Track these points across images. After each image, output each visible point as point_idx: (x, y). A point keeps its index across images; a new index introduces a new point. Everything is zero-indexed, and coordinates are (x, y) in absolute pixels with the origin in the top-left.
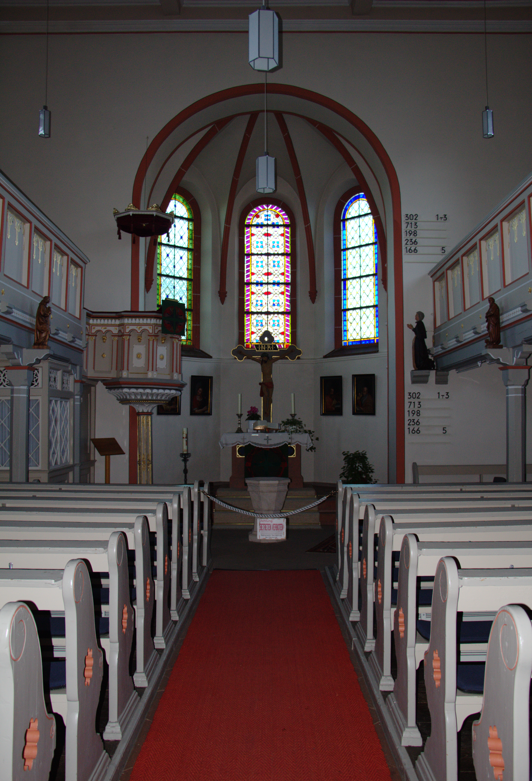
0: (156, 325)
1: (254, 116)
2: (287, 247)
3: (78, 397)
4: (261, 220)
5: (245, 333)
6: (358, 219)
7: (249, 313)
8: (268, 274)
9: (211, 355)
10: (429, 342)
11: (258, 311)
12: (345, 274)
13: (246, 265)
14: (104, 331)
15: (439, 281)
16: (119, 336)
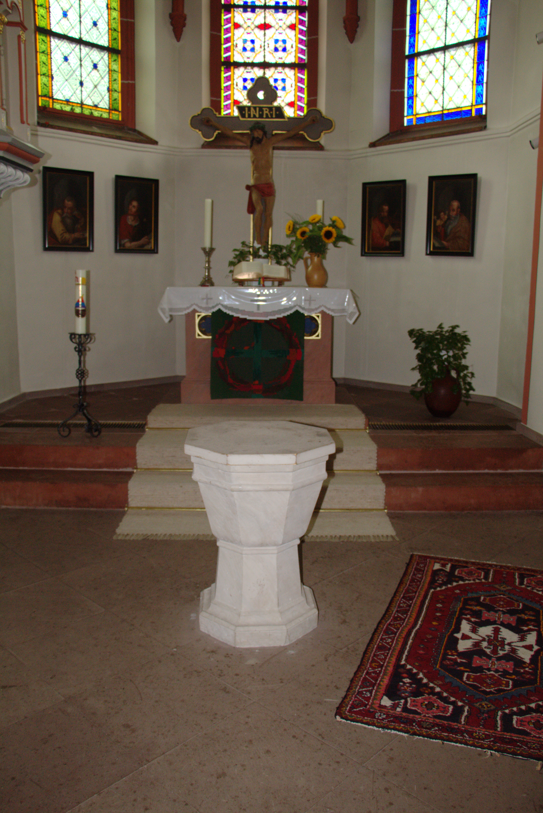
7: (230, 65)
11: (247, 61)
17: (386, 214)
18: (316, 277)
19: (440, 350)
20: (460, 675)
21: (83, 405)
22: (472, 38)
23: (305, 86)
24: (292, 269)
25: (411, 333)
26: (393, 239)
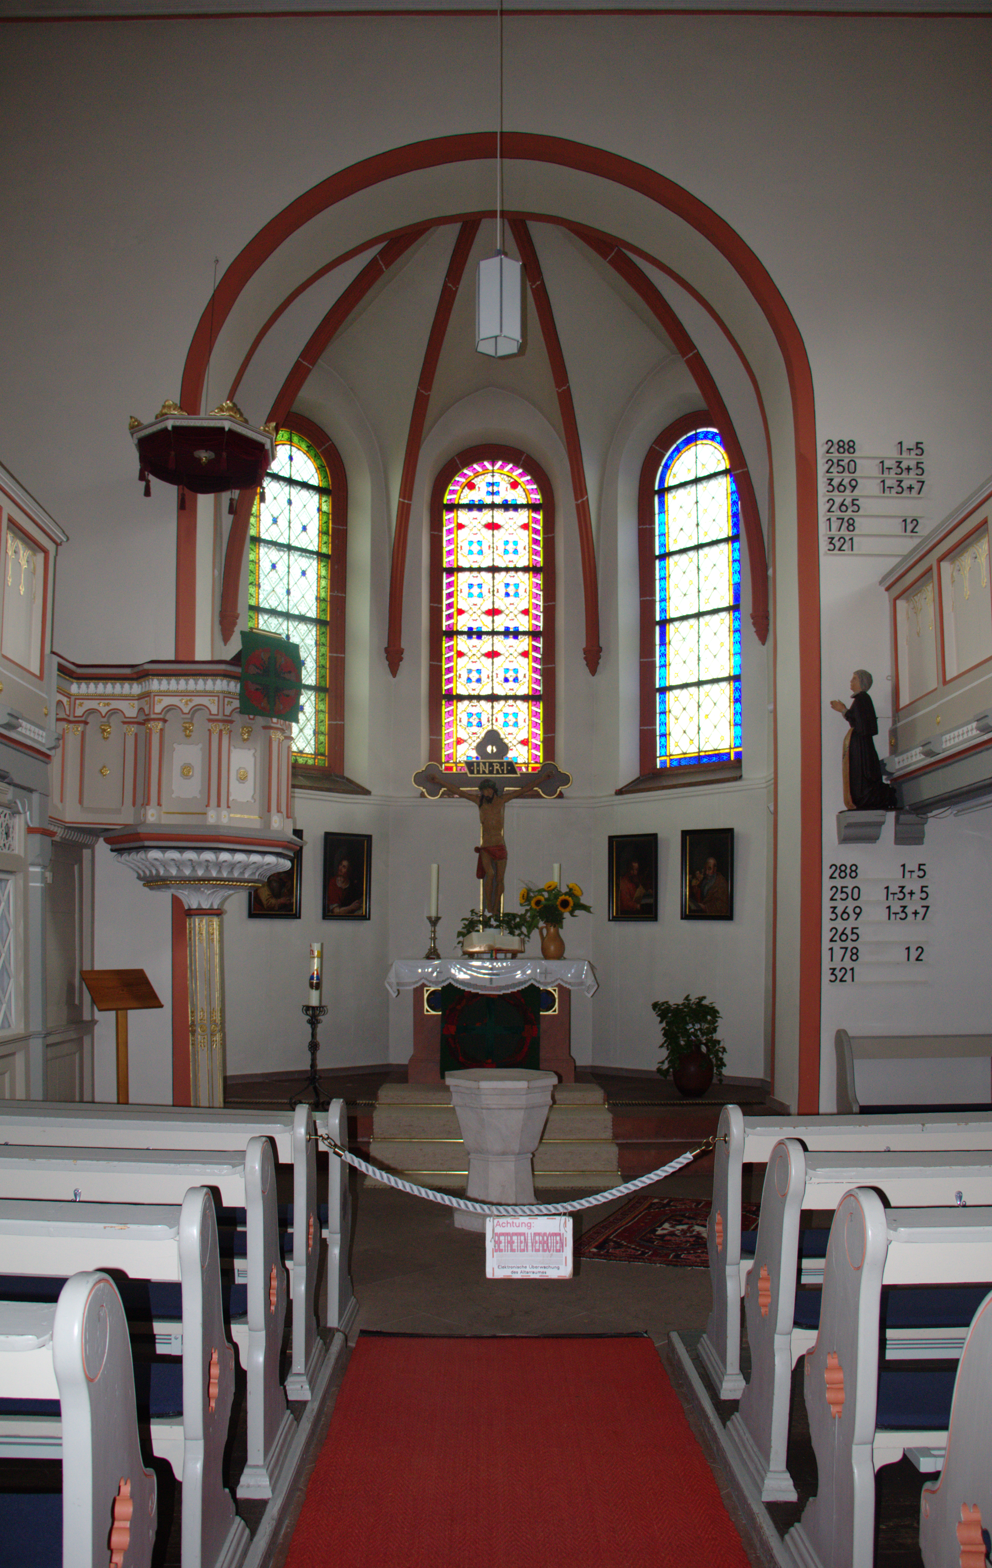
0: (227, 694)
1: (469, 226)
2: (536, 553)
3: (38, 869)
4: (479, 494)
5: (444, 742)
6: (694, 487)
7: (452, 697)
8: (494, 612)
9: (367, 787)
10: (881, 744)
11: (473, 693)
12: (663, 611)
13: (445, 592)
14: (104, 710)
15: (907, 600)
16: (139, 723)
17: (636, 872)
18: (552, 948)
19: (688, 1025)
21: (315, 1078)
22: (727, 675)
23: (540, 721)
24: (527, 939)
25: (655, 1006)
26: (644, 902)
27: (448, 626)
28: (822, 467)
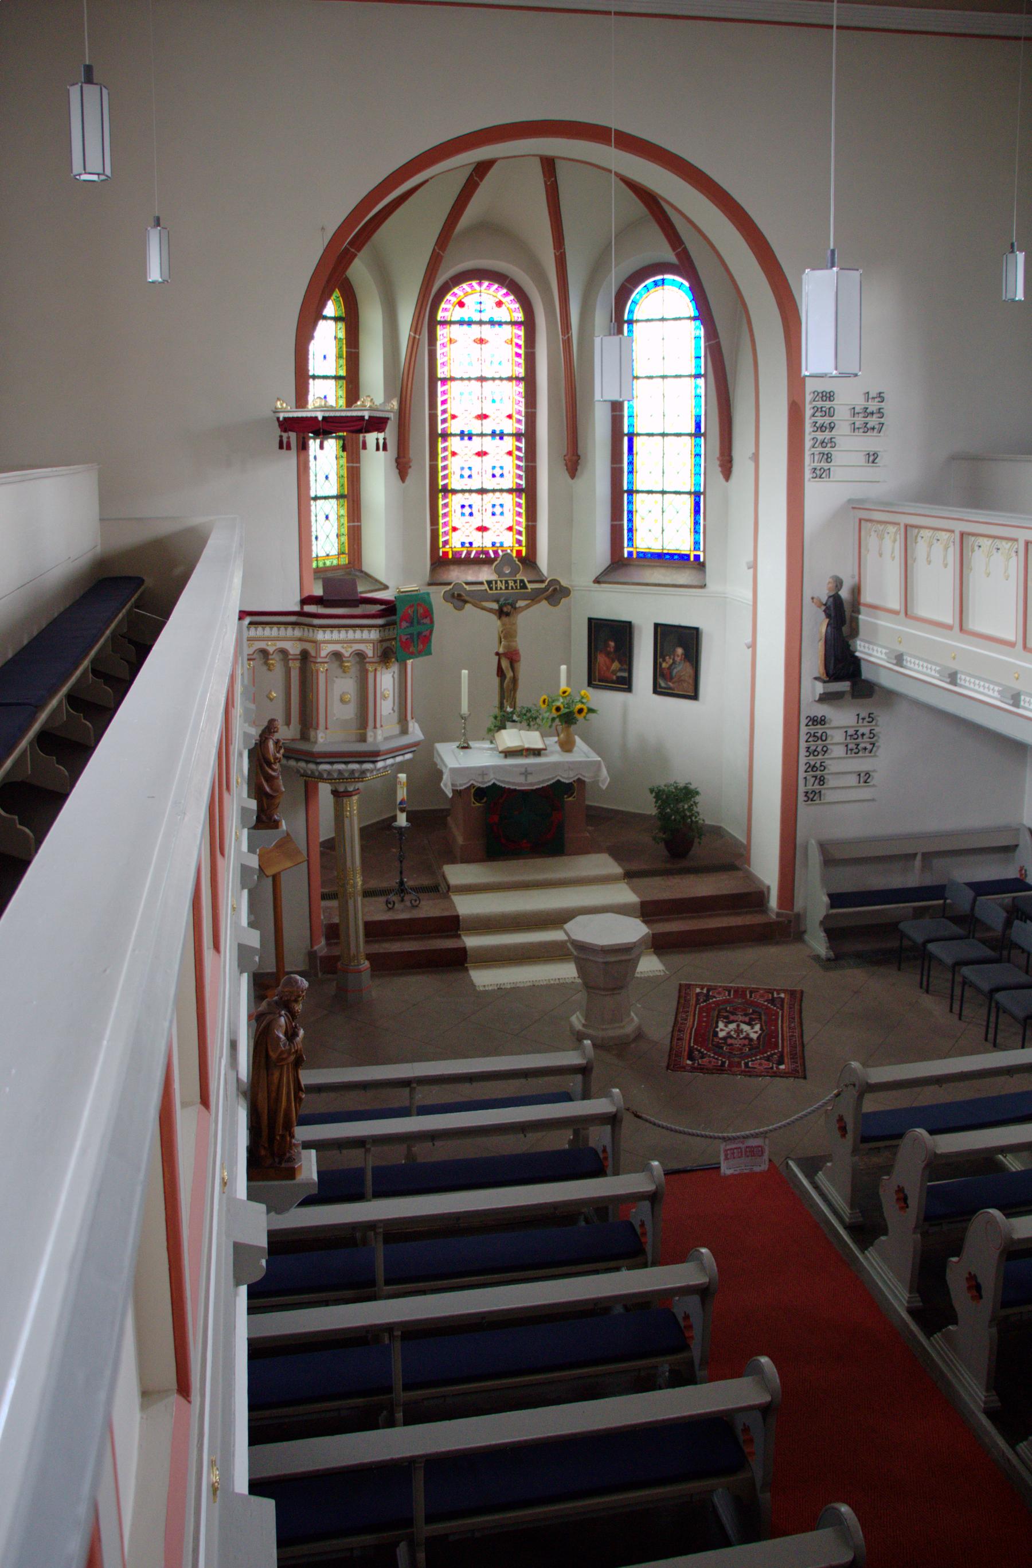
11: (465, 488)
20: (722, 1048)
23: (523, 511)
26: (619, 674)
27: (443, 430)
28: (808, 412)
